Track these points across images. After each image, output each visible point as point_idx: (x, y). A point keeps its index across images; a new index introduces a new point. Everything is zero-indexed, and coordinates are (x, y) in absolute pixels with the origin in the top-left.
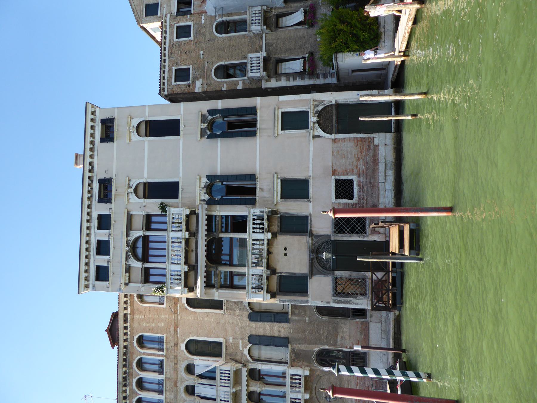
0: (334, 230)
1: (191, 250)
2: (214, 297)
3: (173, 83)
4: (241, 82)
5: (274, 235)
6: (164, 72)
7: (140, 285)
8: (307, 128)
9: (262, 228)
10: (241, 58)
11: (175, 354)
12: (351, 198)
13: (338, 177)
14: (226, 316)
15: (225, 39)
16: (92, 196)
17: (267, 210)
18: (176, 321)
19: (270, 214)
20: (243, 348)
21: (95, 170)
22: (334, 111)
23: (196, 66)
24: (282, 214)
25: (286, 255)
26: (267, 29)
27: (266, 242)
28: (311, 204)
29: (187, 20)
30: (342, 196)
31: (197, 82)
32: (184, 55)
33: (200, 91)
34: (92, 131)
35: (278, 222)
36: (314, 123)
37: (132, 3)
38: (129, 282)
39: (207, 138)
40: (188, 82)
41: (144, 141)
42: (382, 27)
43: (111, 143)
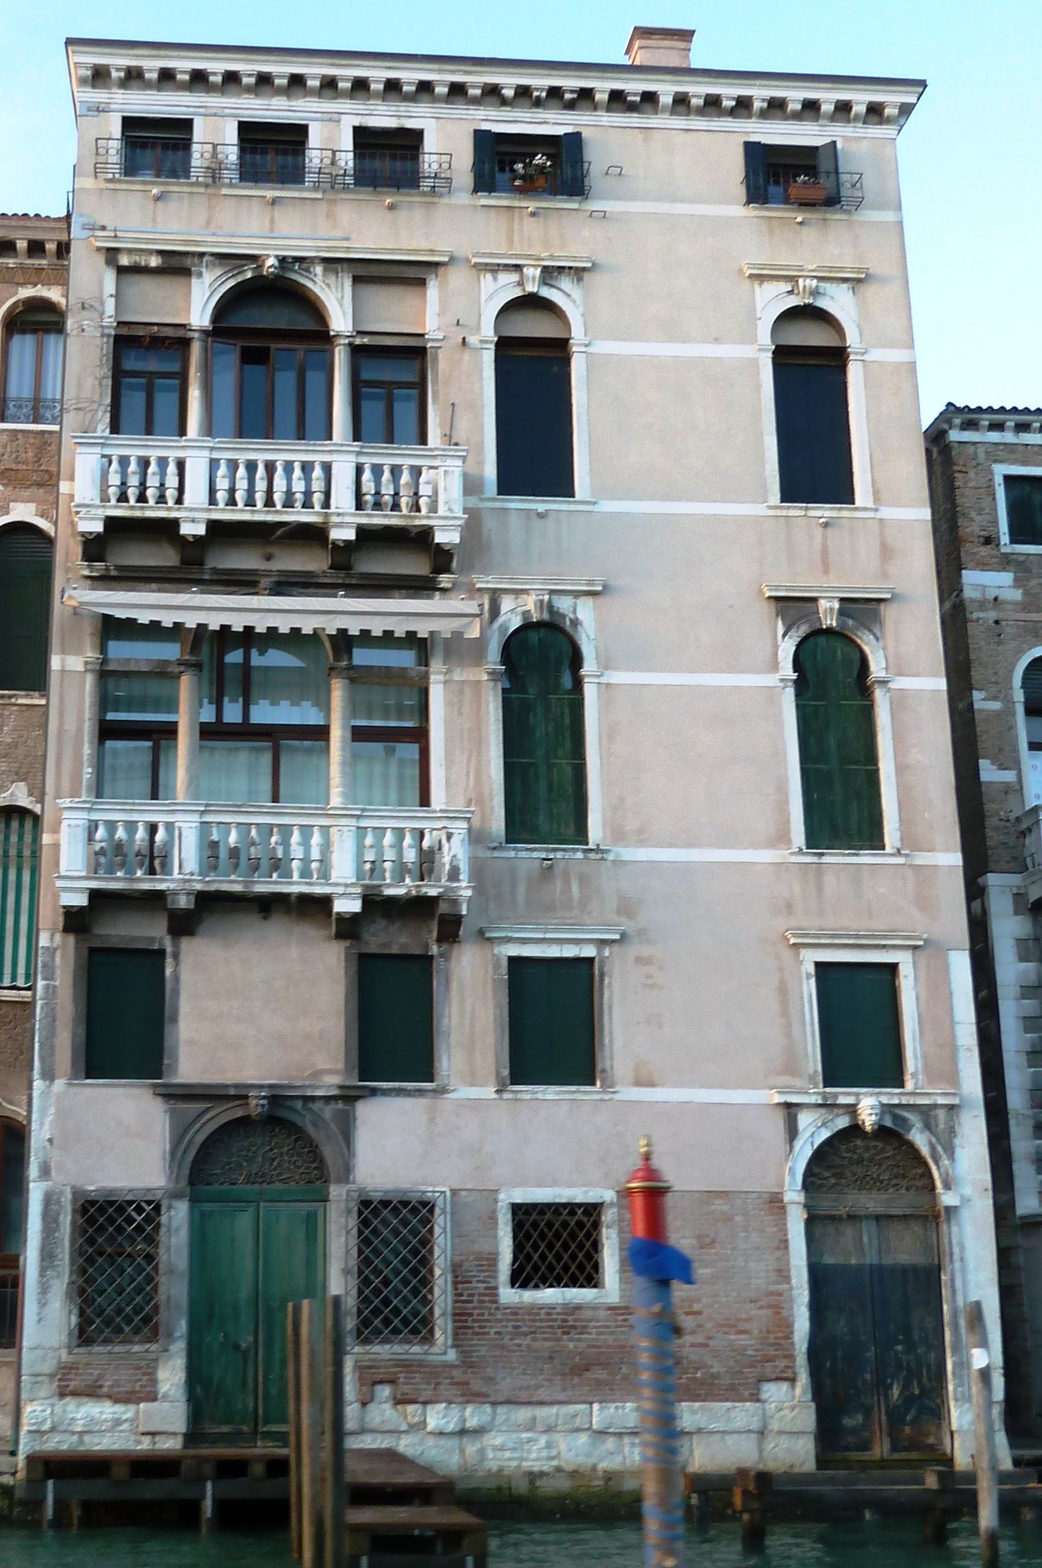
1: (271, 550)
2: (63, 652)
3: (1000, 470)
4: (1009, 776)
5: (348, 928)
7: (109, 321)
8: (833, 1075)
12: (521, 1278)
13: (608, 1216)
16: (504, 102)
17: (465, 890)
19: (443, 908)
24: (438, 964)
30: (528, 1236)
31: (1006, 578)
33: (969, 593)
34: (827, 108)
38: (121, 271)
40: (1005, 539)
41: (753, 340)
43: (741, 192)
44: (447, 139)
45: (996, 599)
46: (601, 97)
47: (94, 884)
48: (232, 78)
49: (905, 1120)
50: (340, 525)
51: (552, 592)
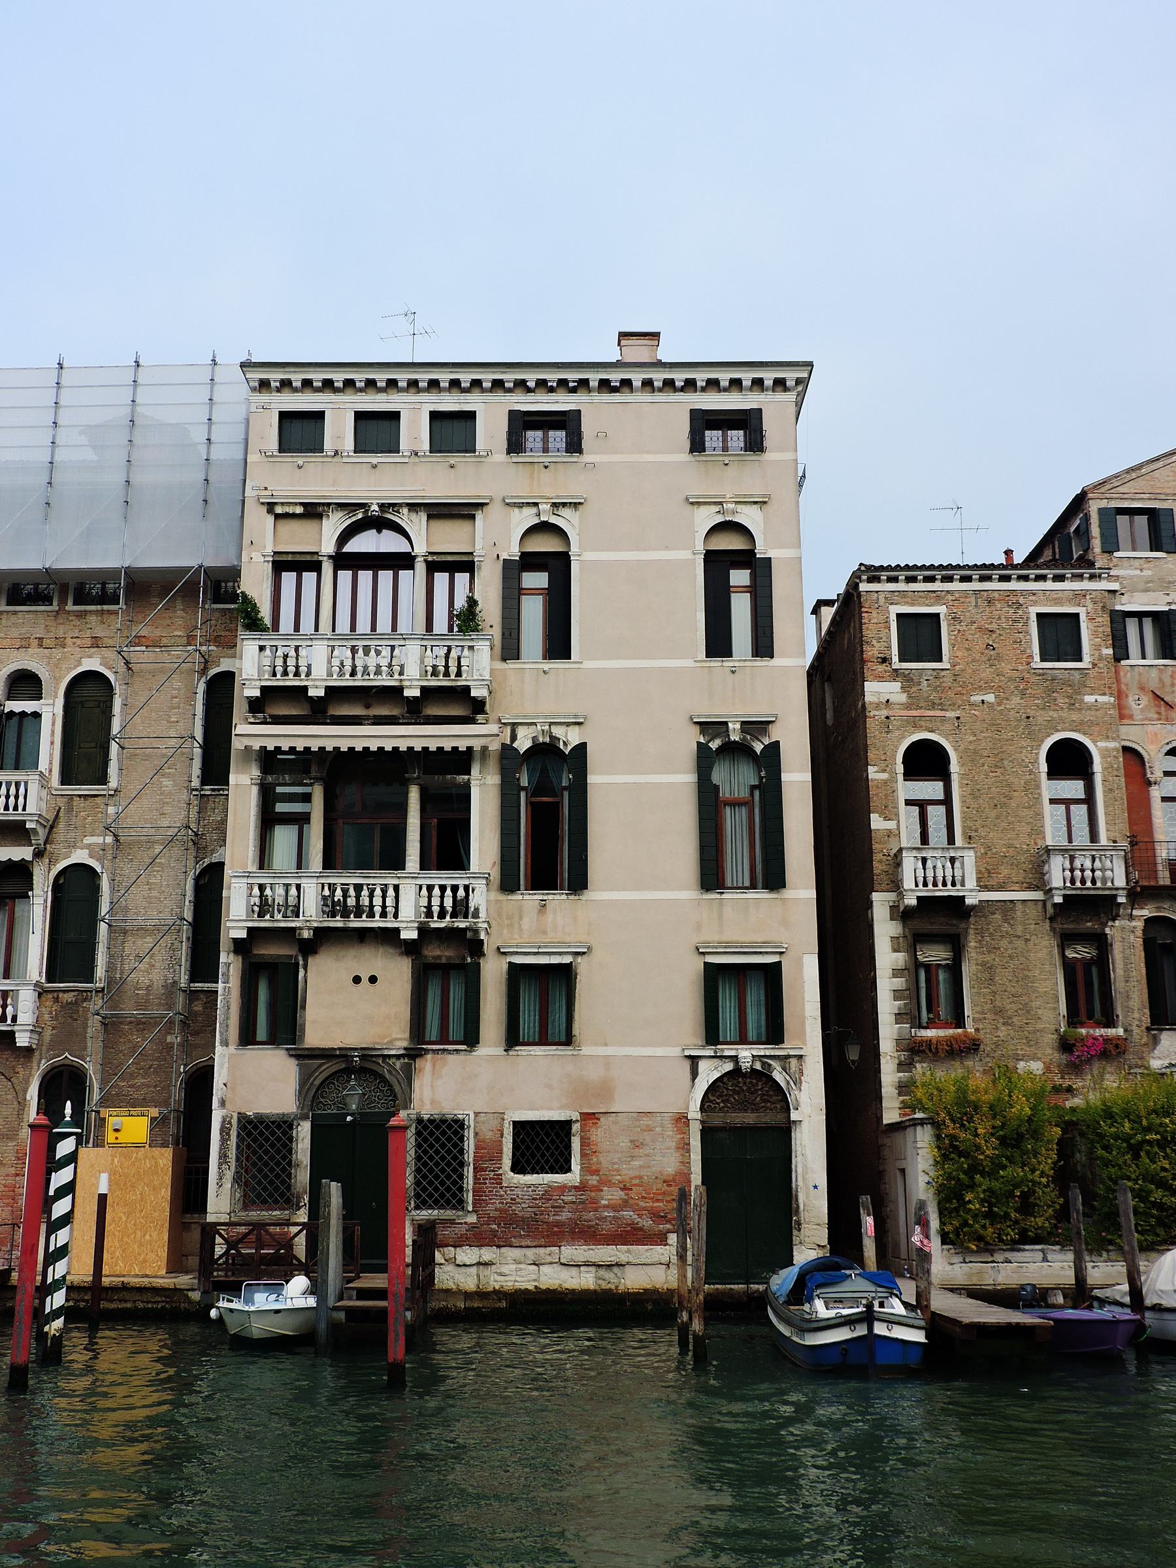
0: (426, 1117)
2: (237, 772)
4: (891, 825)
5: (410, 949)
6: (931, 579)
9: (429, 914)
10: (970, 823)
11: (69, 641)
13: (576, 1128)
14: (184, 796)
15: (1031, 772)
18: (165, 641)
19: (469, 935)
20: (89, 846)
21: (607, 397)
22: (769, 1118)
23: (948, 680)
25: (357, 980)
26: (1055, 905)
27: (390, 924)
28: (500, 1051)
29: (1097, 648)
31: (896, 686)
32: (981, 641)
33: (868, 698)
34: (724, 384)
35: (448, 958)
36: (735, 1059)
37: (1161, 464)
38: (278, 517)
39: (698, 743)
40: (895, 659)
42: (1009, 1255)
44: (491, 417)
45: (888, 701)
46: (594, 384)
47: (250, 924)
48: (349, 383)
49: (770, 1065)
50: (410, 687)
51: (551, 724)
